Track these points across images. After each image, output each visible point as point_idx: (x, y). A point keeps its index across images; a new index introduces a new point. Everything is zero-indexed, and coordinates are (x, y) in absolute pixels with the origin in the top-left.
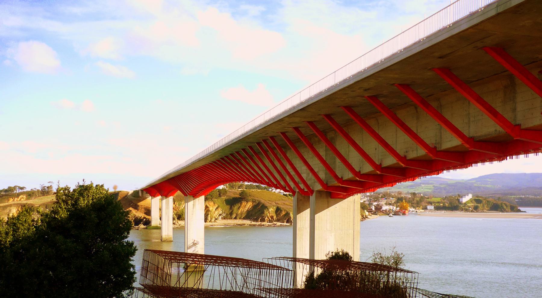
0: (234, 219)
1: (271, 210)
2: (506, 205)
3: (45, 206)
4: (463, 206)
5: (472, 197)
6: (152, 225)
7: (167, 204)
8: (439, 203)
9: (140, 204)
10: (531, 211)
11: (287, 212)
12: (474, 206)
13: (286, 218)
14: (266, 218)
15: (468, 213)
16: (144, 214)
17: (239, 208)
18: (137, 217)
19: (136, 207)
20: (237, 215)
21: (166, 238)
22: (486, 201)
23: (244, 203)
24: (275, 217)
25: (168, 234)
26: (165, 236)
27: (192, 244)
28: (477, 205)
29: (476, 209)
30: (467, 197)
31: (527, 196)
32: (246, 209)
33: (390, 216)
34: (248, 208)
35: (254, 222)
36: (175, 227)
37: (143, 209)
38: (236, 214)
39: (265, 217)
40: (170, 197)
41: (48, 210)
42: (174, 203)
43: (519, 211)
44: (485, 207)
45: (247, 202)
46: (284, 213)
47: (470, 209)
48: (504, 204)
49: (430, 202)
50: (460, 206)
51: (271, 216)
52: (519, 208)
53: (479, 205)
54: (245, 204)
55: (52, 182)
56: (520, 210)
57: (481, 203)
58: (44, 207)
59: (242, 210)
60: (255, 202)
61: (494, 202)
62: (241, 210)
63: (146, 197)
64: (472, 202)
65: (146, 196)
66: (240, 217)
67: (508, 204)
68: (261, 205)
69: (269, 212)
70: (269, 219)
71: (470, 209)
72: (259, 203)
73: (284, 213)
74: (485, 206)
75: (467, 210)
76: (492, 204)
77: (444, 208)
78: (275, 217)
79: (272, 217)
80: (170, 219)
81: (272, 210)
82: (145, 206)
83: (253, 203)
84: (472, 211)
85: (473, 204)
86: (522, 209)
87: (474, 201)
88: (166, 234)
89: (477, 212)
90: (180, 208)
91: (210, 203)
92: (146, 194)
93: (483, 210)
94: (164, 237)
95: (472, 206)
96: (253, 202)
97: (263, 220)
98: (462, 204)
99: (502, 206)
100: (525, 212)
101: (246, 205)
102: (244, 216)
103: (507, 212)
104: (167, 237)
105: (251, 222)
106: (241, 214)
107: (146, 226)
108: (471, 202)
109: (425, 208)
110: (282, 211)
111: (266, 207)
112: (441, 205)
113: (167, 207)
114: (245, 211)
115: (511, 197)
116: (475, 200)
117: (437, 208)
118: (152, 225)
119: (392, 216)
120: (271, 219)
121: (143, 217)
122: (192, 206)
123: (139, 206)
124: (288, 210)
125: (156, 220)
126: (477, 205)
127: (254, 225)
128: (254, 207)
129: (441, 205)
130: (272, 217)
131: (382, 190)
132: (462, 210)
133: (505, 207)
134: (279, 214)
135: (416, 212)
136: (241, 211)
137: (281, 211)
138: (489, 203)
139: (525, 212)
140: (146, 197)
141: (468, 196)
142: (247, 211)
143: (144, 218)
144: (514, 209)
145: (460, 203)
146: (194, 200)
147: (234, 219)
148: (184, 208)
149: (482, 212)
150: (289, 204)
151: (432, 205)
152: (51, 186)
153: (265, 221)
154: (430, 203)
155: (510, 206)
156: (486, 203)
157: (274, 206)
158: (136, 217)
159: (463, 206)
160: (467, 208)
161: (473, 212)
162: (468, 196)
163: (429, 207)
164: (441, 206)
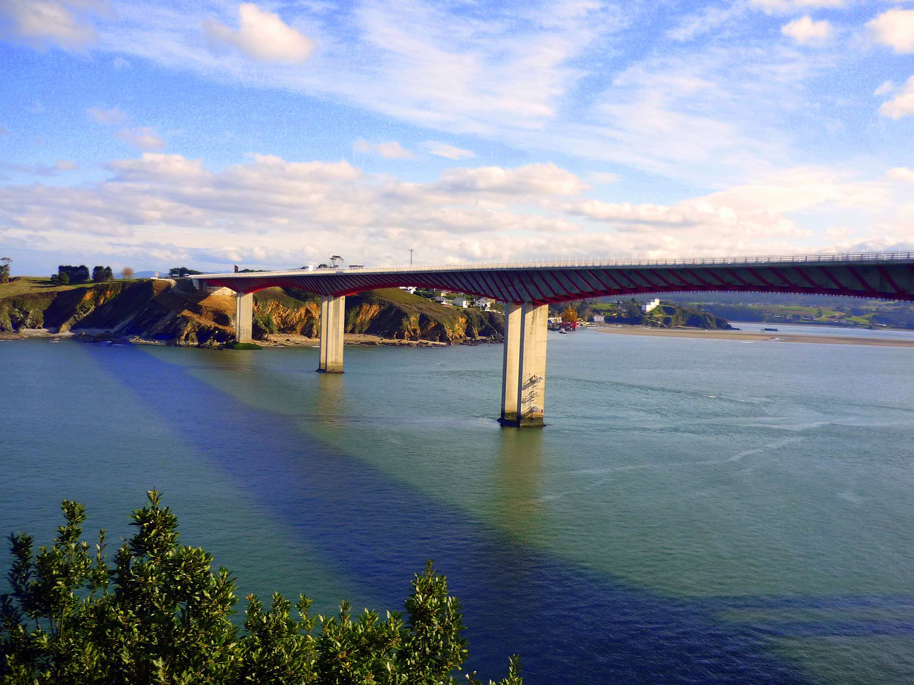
0: (349, 332)
1: (413, 319)
2: (711, 320)
3: (12, 302)
4: (648, 318)
5: (660, 304)
6: (240, 342)
7: (337, 308)
8: (610, 312)
9: (204, 303)
10: (745, 327)
11: (439, 324)
12: (663, 319)
13: (438, 333)
14: (406, 333)
15: (655, 330)
16: (214, 321)
17: (357, 315)
18: (203, 327)
19: (197, 310)
20: (354, 325)
21: (333, 366)
22: (680, 311)
23: (366, 307)
24: (418, 331)
25: (336, 359)
26: (332, 362)
27: (529, 382)
28: (667, 316)
29: (667, 323)
30: (652, 303)
31: (741, 304)
32: (370, 316)
33: (560, 332)
34: (373, 315)
35: (385, 338)
36: (269, 346)
37: (210, 314)
38: (353, 325)
39: (405, 331)
40: (342, 297)
41: (17, 309)
42: (256, 305)
43: (729, 327)
44: (680, 321)
45: (371, 305)
46: (433, 325)
47: (659, 322)
48: (708, 316)
49: (596, 309)
50: (645, 318)
51: (414, 329)
52: (728, 324)
53: (671, 316)
54: (368, 308)
55: (9, 259)
56: (731, 327)
57: (673, 314)
58: (10, 305)
59: (362, 318)
60: (383, 305)
61: (693, 313)
62: (360, 318)
63: (208, 292)
64: (659, 311)
65: (208, 290)
66: (360, 330)
67: (713, 316)
68: (395, 310)
69: (410, 323)
70: (411, 335)
71: (659, 322)
72: (391, 307)
73: (433, 325)
74: (680, 318)
75: (654, 325)
76: (690, 316)
77: (619, 320)
78: (418, 331)
79: (415, 331)
80: (340, 334)
81: (414, 319)
82: (212, 307)
83: (380, 307)
84: (662, 326)
85: (662, 315)
86: (733, 324)
87: (662, 310)
88: (334, 360)
89: (669, 327)
90: (264, 312)
91: (312, 306)
92: (208, 287)
93: (676, 325)
94: (330, 365)
95: (662, 317)
96: (380, 305)
97: (401, 336)
98: (646, 314)
99: (705, 320)
100: (738, 329)
101: (369, 310)
102: (366, 328)
103: (712, 328)
104: (334, 365)
105: (382, 339)
106: (362, 324)
107: (219, 343)
108: (658, 312)
109: (591, 320)
110: (430, 321)
111: (405, 315)
112: (614, 314)
113: (336, 315)
114: (367, 319)
115: (693, 305)
116: (664, 308)
117: (609, 320)
118: (240, 342)
119: (565, 332)
120: (413, 335)
121: (213, 327)
122: (532, 319)
123: (201, 307)
124: (439, 321)
125: (247, 333)
126: (667, 316)
127: (387, 344)
128: (382, 314)
129: (614, 314)
130: (415, 331)
131: (693, 300)
132: (647, 325)
133: (709, 321)
134: (426, 326)
135: (581, 325)
136: (361, 320)
137: (429, 321)
138: (685, 314)
139: (738, 329)
140: (208, 292)
141: (654, 301)
142: (370, 319)
143: (216, 328)
144: (722, 325)
145: (644, 313)
146: (534, 309)
147: (349, 332)
148: (270, 312)
149: (676, 328)
150: (436, 310)
151: (600, 315)
152: (5, 266)
153: (405, 337)
154: (597, 312)
155: (715, 319)
156: (681, 314)
157: (416, 312)
158: (201, 327)
159: (648, 318)
160: (655, 321)
161: (664, 327)
162: (654, 301)
163: (597, 318)
164: (615, 316)
